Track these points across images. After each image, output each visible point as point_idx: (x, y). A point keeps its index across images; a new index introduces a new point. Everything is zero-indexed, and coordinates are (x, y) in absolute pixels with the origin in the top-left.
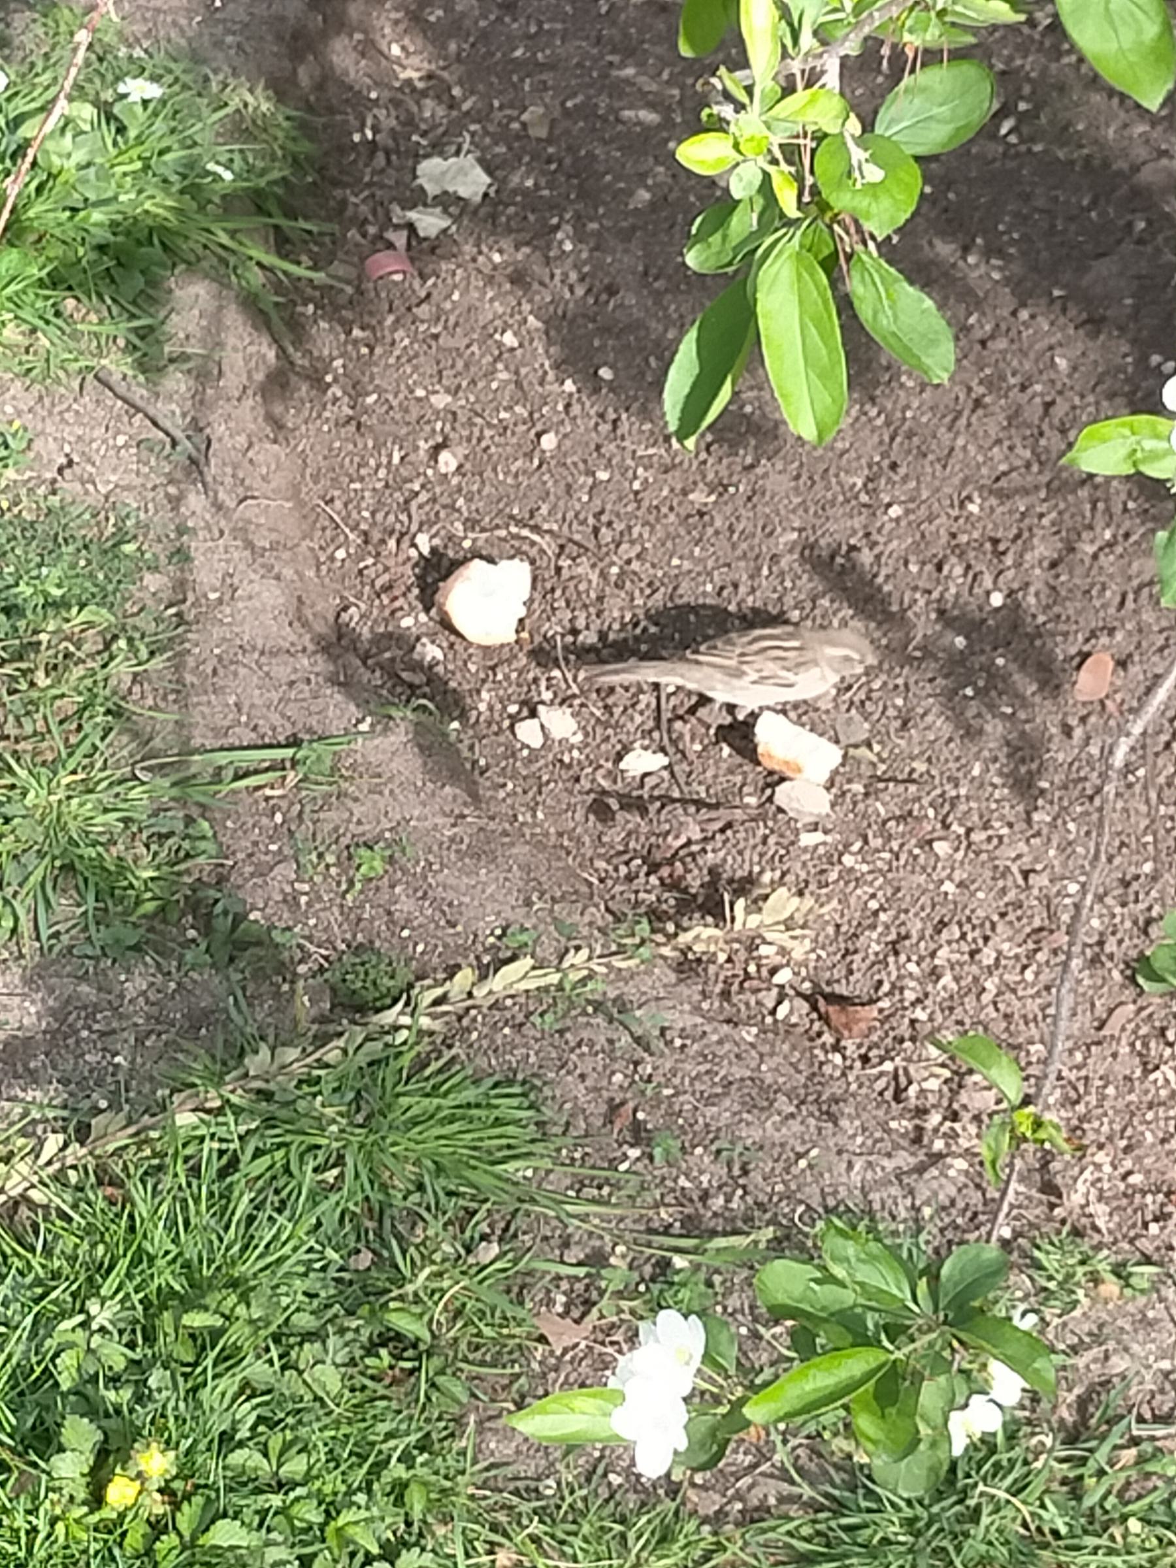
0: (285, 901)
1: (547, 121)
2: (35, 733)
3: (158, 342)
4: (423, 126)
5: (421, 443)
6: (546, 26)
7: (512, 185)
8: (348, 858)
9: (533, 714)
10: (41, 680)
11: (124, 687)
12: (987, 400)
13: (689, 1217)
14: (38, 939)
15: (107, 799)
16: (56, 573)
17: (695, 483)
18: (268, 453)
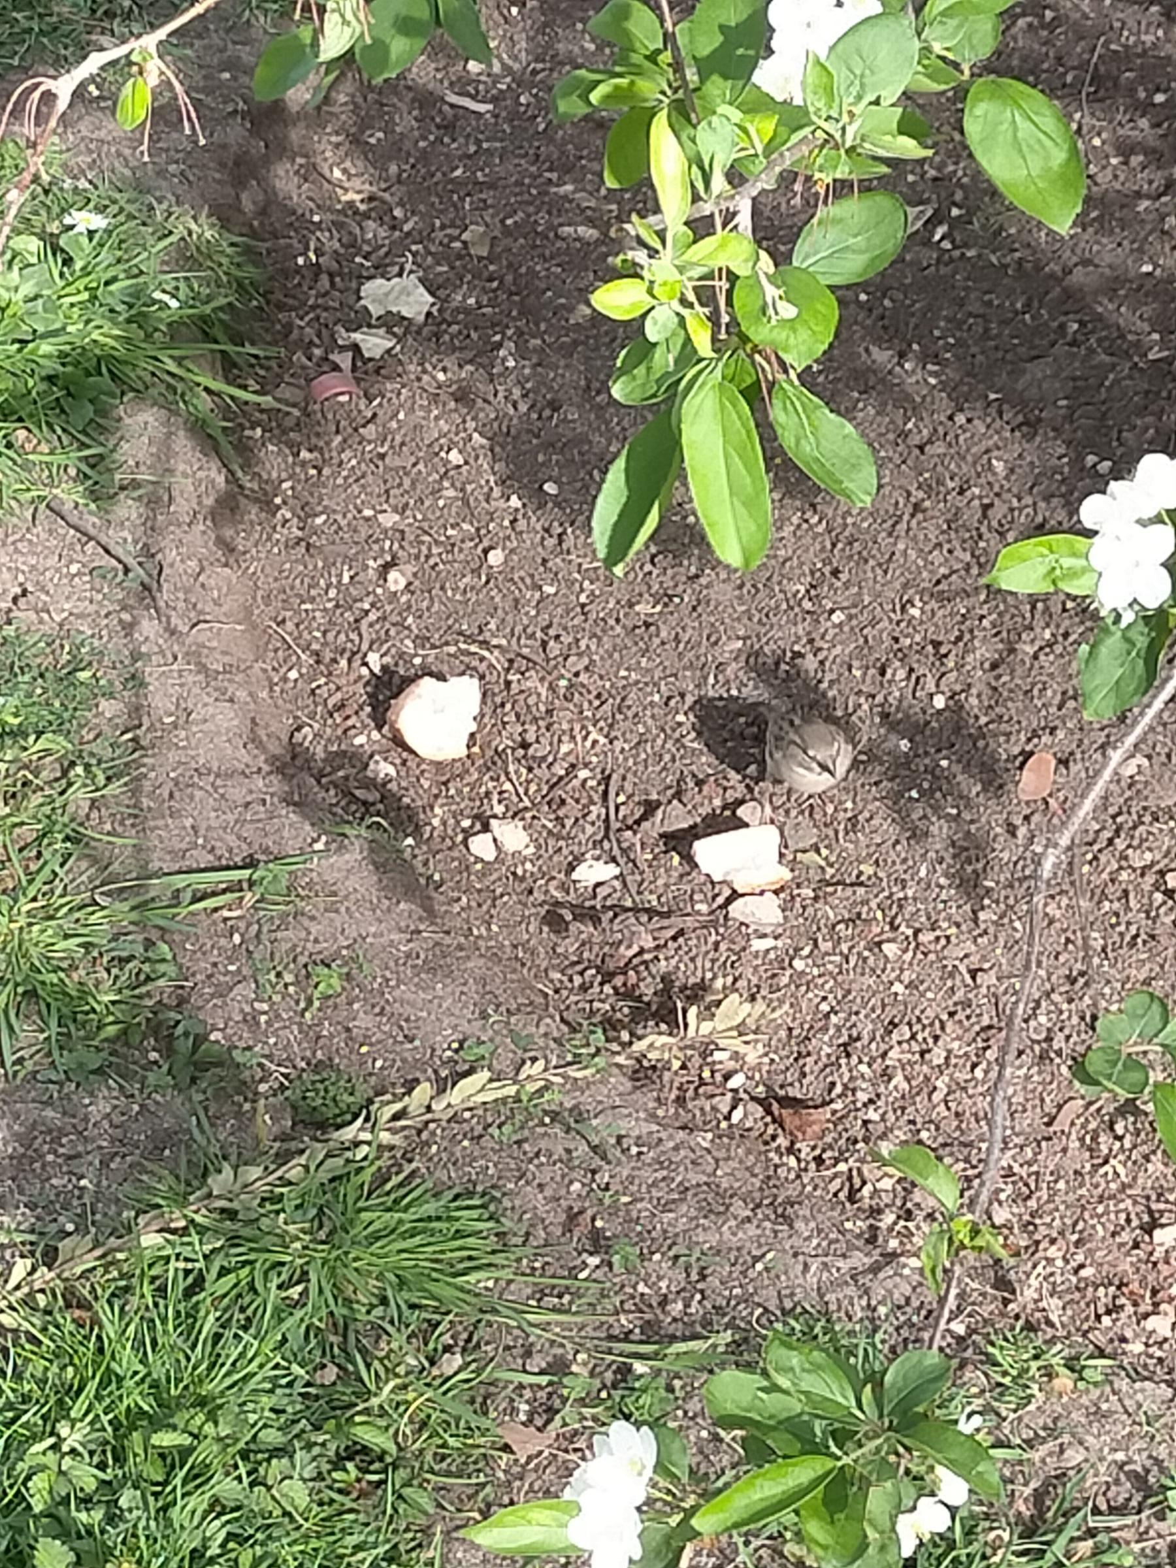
1: (488, 241)
3: (109, 470)
4: (366, 248)
5: (371, 563)
6: (485, 145)
7: (454, 304)
8: (305, 977)
9: (486, 828)
11: (82, 813)
12: (927, 504)
15: (67, 925)
18: (220, 577)
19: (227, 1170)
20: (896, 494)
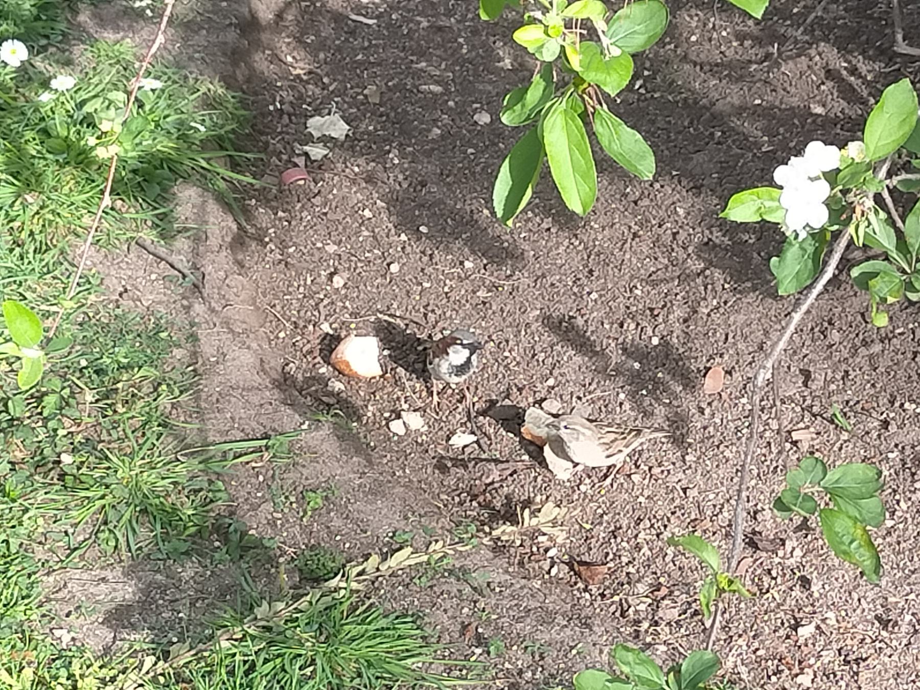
0: (268, 523)
1: (378, 94)
2: (119, 439)
3: (170, 222)
4: (309, 100)
5: (323, 272)
6: (374, 42)
7: (361, 130)
8: (302, 498)
9: (399, 417)
10: (120, 409)
11: (167, 411)
12: (641, 233)
13: (512, 683)
14: (130, 551)
15: (163, 472)
16: (123, 350)
17: (480, 287)
18: (237, 280)
19: (265, 604)
20: (622, 228)
